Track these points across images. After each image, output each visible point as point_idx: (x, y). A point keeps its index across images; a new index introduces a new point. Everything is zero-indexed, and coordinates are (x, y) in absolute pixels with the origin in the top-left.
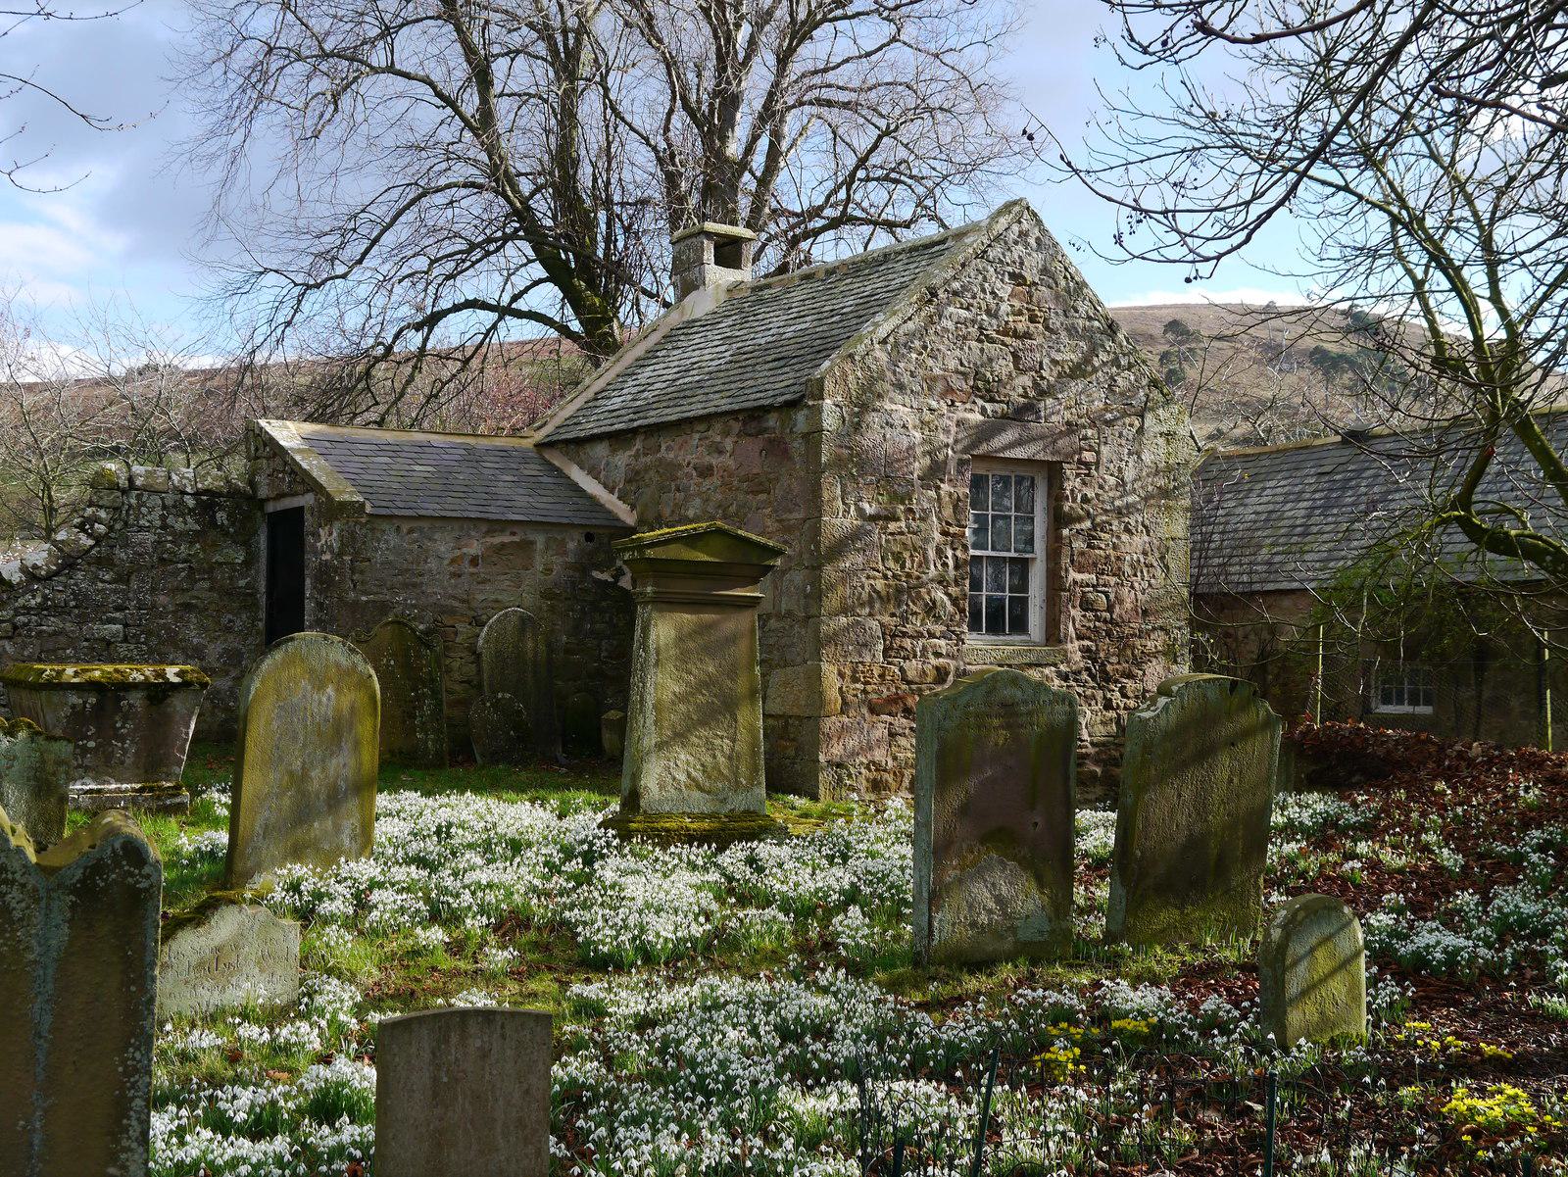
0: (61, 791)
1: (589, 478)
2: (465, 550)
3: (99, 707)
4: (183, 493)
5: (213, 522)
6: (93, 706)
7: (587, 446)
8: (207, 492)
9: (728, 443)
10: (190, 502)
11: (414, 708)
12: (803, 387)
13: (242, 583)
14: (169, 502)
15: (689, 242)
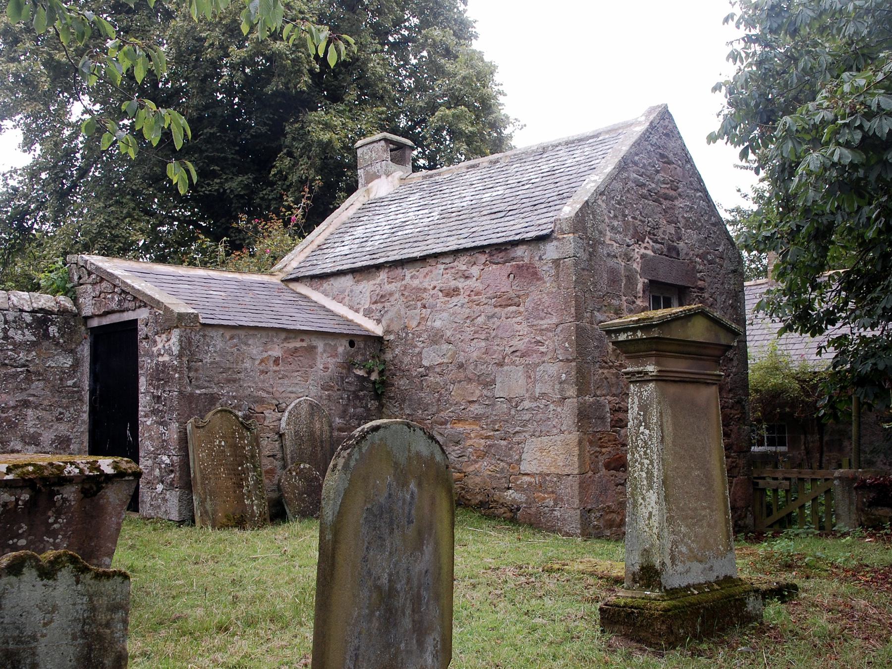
0: (118, 647)
1: (334, 302)
2: (270, 353)
3: (31, 505)
4: (22, 311)
5: (46, 335)
6: (25, 503)
7: (332, 279)
8: (41, 310)
9: (475, 271)
10: (28, 318)
11: (241, 480)
12: (552, 225)
13: (70, 383)
14: (10, 318)
15: (371, 146)
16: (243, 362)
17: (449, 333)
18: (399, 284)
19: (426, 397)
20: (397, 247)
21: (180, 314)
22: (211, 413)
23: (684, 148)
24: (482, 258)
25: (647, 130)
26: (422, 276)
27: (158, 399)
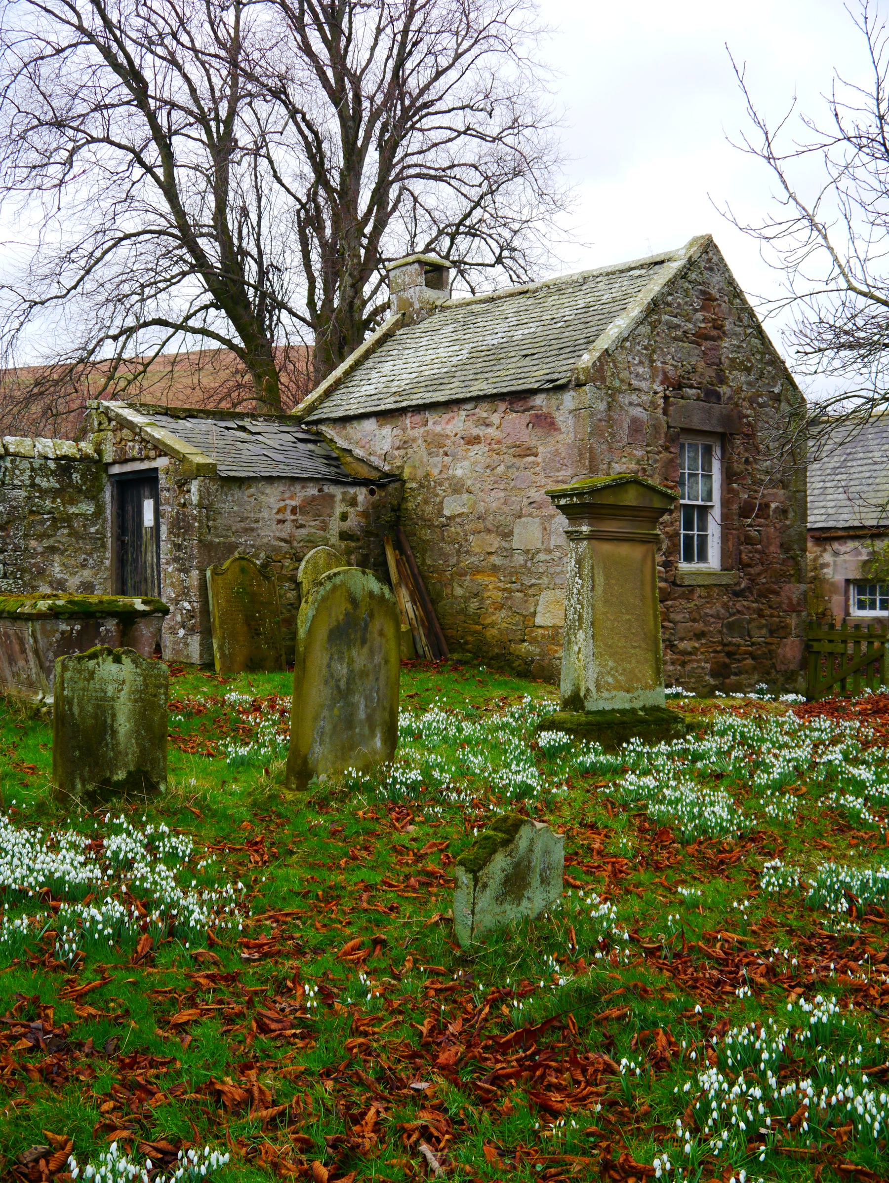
2: (287, 502)
4: (46, 458)
6: (78, 632)
8: (65, 457)
9: (495, 418)
10: (52, 465)
13: (93, 530)
14: (36, 465)
15: (404, 269)
16: (260, 511)
17: (469, 483)
18: (422, 430)
19: (447, 548)
20: (422, 390)
21: (198, 465)
22: (228, 562)
23: (731, 282)
24: (502, 406)
25: (684, 267)
26: (443, 422)
27: (178, 547)
